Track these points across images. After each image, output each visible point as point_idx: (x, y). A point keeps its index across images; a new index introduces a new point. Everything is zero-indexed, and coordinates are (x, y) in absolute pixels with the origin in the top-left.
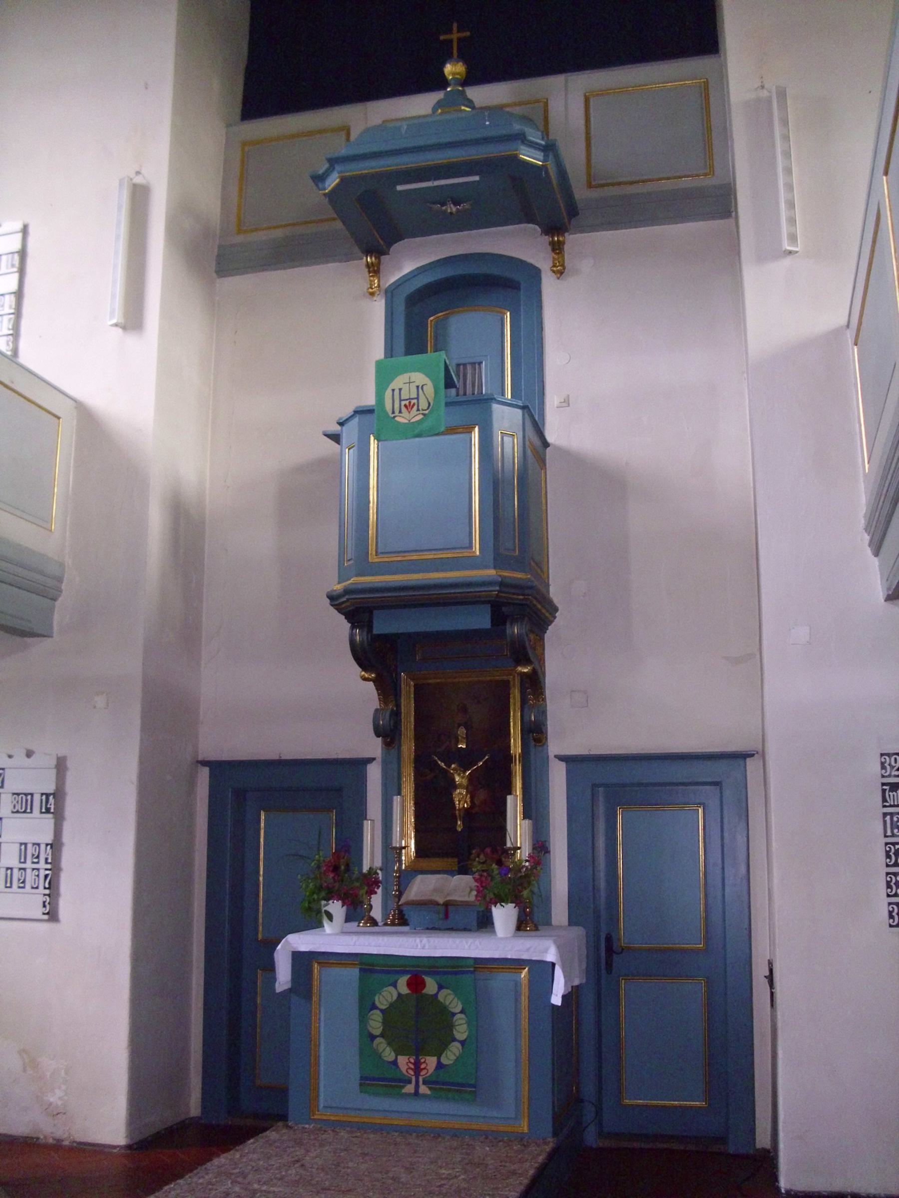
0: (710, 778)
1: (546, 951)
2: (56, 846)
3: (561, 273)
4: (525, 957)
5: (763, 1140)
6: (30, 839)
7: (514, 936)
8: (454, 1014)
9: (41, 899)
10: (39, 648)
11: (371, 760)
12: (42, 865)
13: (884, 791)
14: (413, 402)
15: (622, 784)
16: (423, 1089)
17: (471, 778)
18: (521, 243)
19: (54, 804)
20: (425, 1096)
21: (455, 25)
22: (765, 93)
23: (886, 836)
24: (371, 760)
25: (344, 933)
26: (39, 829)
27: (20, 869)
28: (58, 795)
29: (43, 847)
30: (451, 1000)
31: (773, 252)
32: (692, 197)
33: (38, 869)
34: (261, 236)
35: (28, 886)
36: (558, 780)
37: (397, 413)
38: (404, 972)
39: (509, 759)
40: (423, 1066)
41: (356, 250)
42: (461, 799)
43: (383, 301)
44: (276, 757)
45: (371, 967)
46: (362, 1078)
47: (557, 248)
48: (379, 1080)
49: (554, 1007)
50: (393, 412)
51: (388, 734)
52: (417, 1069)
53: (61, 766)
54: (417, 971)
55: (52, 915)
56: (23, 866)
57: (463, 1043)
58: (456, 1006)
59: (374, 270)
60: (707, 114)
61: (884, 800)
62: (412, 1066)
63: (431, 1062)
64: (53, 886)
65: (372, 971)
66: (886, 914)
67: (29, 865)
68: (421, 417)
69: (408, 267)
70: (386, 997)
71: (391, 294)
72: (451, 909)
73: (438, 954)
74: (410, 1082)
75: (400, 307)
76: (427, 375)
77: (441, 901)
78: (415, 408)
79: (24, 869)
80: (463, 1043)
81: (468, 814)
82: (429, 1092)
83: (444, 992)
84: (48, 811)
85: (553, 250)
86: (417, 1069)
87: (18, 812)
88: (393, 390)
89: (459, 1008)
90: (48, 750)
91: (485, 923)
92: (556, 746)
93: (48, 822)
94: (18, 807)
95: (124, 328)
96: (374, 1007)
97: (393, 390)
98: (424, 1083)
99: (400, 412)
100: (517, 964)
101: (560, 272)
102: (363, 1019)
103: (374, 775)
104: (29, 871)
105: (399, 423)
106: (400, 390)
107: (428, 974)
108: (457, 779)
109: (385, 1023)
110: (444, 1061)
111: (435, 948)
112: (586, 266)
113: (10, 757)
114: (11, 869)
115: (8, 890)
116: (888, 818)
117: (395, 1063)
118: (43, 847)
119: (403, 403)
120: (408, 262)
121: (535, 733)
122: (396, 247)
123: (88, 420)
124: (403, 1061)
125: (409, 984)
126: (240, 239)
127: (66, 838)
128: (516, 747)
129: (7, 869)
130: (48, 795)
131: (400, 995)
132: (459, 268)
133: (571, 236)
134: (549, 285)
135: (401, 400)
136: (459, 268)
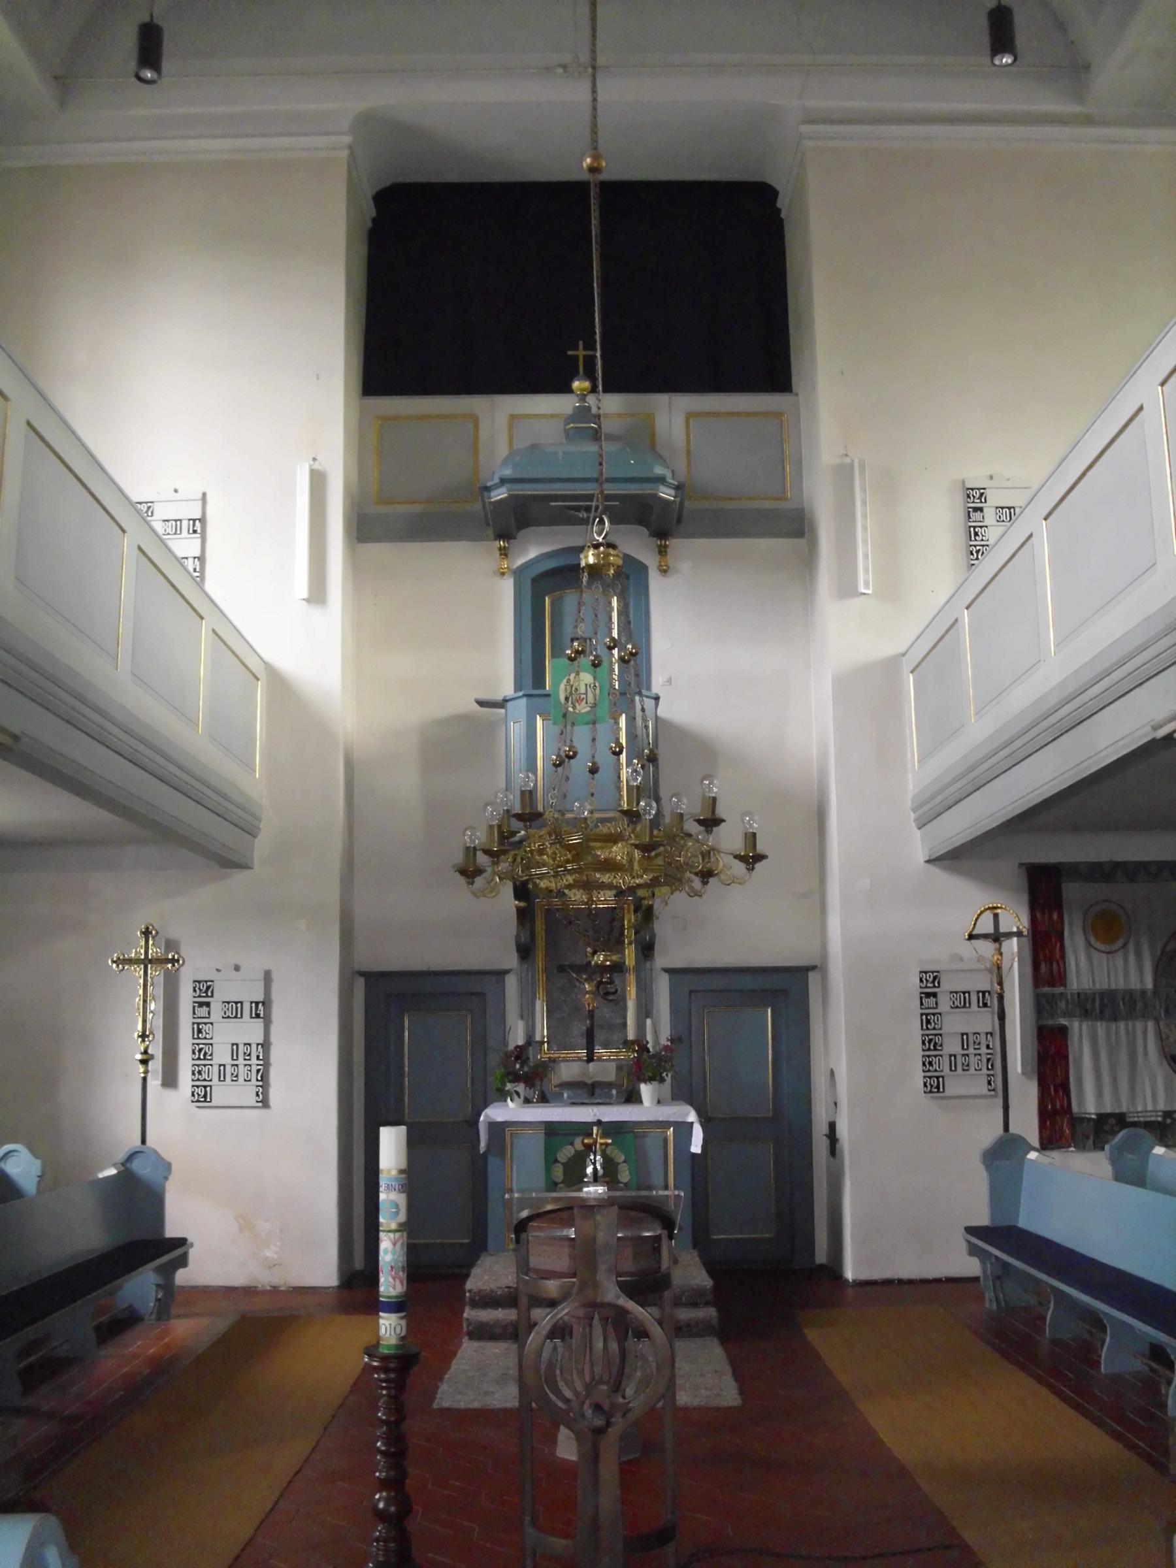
0: (784, 991)
1: (687, 1114)
2: (266, 1045)
3: (665, 571)
5: (821, 1257)
6: (241, 1040)
9: (255, 1089)
10: (239, 878)
11: (507, 972)
12: (254, 1061)
18: (636, 544)
19: (262, 1010)
21: (581, 343)
22: (847, 460)
24: (507, 972)
26: (250, 1031)
28: (266, 1003)
29: (254, 1047)
31: (847, 589)
32: (773, 523)
34: (401, 509)
35: (241, 1079)
36: (662, 988)
41: (490, 532)
43: (512, 580)
44: (423, 968)
45: (552, 1130)
47: (662, 551)
49: (694, 1155)
51: (525, 952)
53: (268, 977)
55: (265, 1103)
59: (504, 553)
60: (783, 451)
61: (922, 1004)
64: (264, 1078)
67: (241, 1061)
69: (533, 553)
71: (518, 573)
75: (528, 586)
77: (589, 1082)
84: (258, 1016)
85: (660, 552)
89: (623, 1158)
90: (254, 964)
91: (632, 1097)
92: (663, 959)
93: (259, 1024)
94: (957, 1003)
95: (308, 600)
96: (556, 1161)
100: (666, 1124)
101: (664, 571)
102: (548, 1171)
104: (972, 1057)
109: (565, 1173)
112: (684, 567)
113: (218, 970)
118: (254, 1047)
120: (533, 549)
121: (647, 950)
122: (521, 534)
123: (277, 681)
126: (382, 509)
127: (274, 1038)
130: (257, 1003)
132: (581, 564)
133: (1071, 885)
134: (656, 583)
136: (581, 564)
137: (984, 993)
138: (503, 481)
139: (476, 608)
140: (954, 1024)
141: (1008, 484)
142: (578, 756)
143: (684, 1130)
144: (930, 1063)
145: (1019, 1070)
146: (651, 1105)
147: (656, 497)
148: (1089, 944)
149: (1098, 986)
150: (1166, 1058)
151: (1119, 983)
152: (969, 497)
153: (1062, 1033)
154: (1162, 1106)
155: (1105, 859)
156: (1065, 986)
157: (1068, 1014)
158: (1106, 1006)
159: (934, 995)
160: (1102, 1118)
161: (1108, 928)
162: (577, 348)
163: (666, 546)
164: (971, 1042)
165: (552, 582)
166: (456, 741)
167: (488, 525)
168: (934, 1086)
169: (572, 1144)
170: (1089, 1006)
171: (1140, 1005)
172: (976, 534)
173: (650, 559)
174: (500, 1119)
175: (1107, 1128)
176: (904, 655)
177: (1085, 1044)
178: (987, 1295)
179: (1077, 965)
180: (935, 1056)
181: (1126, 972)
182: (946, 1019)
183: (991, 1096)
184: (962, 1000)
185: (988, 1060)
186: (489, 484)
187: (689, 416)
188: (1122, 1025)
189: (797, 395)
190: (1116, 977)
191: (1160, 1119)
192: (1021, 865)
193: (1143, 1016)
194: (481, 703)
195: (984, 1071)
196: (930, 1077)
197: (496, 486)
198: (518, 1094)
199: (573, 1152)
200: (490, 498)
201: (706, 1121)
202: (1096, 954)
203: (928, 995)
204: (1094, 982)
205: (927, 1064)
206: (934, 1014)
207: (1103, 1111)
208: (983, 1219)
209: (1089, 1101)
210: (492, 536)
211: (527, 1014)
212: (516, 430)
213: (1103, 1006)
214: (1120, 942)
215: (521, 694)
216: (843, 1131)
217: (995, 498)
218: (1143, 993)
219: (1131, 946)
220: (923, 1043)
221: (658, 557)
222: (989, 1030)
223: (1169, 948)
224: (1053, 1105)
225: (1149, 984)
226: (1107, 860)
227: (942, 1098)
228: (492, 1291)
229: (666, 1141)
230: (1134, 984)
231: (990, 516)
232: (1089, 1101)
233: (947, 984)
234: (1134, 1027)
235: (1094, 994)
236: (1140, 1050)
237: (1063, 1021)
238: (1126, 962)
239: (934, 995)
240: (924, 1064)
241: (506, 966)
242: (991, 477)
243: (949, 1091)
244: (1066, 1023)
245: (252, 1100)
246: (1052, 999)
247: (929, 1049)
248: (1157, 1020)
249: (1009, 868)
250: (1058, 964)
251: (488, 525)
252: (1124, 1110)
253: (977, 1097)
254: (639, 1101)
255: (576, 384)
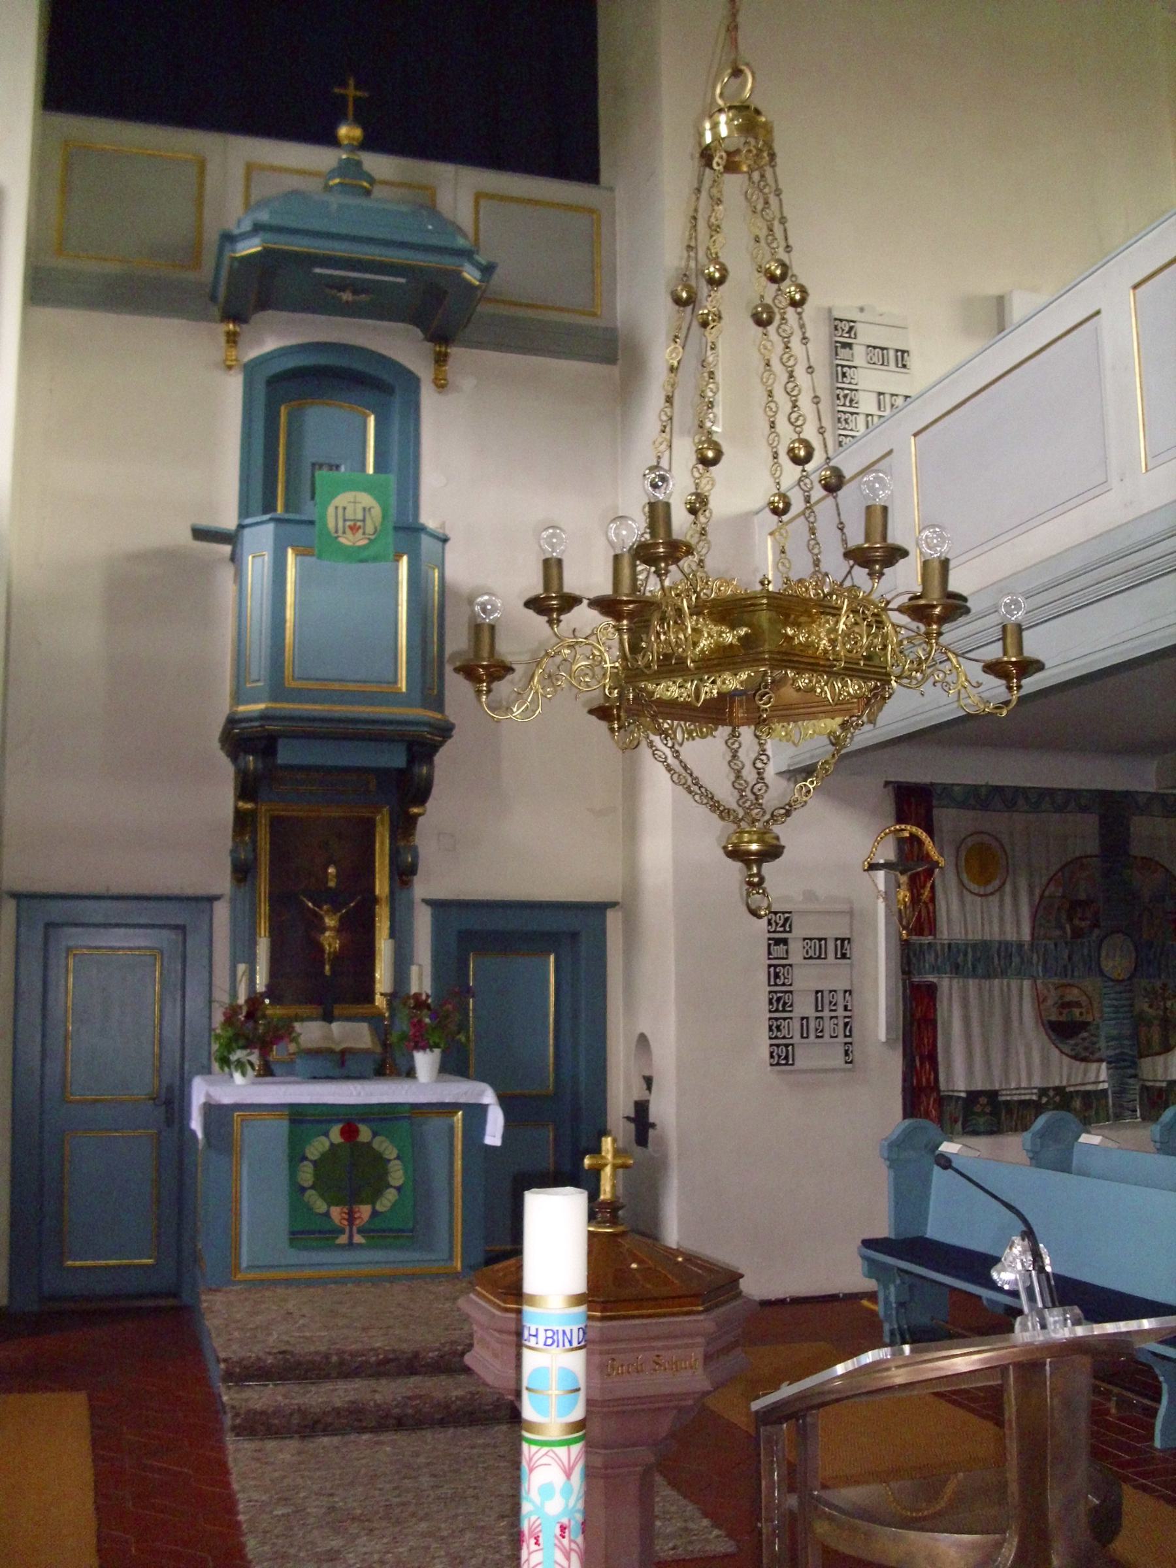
1: (481, 1094)
3: (442, 386)
4: (462, 1100)
6: (825, 986)
7: (438, 1081)
8: (389, 1161)
11: (217, 898)
13: (769, 945)
14: (359, 524)
15: (487, 933)
16: (358, 1239)
17: (342, 921)
20: (360, 1246)
23: (769, 985)
24: (217, 898)
25: (253, 1083)
27: (817, 1018)
30: (387, 1148)
33: (836, 1017)
35: (827, 1036)
37: (340, 533)
38: (339, 1121)
39: (375, 900)
40: (356, 1215)
41: (216, 311)
42: (330, 941)
46: (293, 1233)
47: (441, 359)
48: (308, 1232)
50: (336, 532)
51: (242, 872)
52: (351, 1219)
54: (350, 1119)
56: (819, 1014)
57: (399, 1189)
58: (390, 1152)
59: (232, 339)
61: (769, 953)
62: (346, 1216)
63: (365, 1211)
65: (301, 1122)
66: (767, 1055)
68: (366, 541)
69: (270, 345)
70: (317, 1147)
71: (250, 370)
72: (347, 1056)
73: (374, 1100)
74: (342, 1231)
76: (377, 499)
77: (338, 1048)
78: (361, 531)
79: (821, 1018)
80: (399, 1189)
81: (337, 958)
82: (363, 1241)
83: (378, 1139)
86: (351, 1219)
87: (811, 958)
88: (337, 508)
89: (394, 1155)
92: (423, 888)
94: (811, 953)
96: (304, 1158)
97: (337, 508)
98: (360, 1231)
99: (344, 532)
100: (449, 1109)
101: (441, 385)
103: (222, 913)
104: (827, 1021)
105: (341, 544)
106: (345, 509)
107: (363, 1121)
108: (327, 920)
109: (317, 1176)
110: (379, 1207)
111: (371, 1095)
112: (467, 383)
114: (807, 1018)
115: (820, 1040)
116: (772, 969)
117: (327, 1214)
119: (348, 523)
120: (272, 338)
121: (404, 873)
124: (337, 1213)
125: (343, 1133)
128: (382, 887)
129: (803, 1019)
131: (332, 1144)
135: (345, 520)
137: (843, 940)
138: (258, 228)
139: (189, 410)
140: (806, 979)
141: (878, 320)
142: (724, 460)
143: (476, 1114)
144: (778, 1028)
145: (882, 1036)
146: (426, 1081)
147: (457, 274)
148: (961, 882)
149: (970, 937)
150: (1043, 1025)
151: (993, 933)
152: (836, 328)
153: (930, 991)
154: (1037, 1082)
155: (981, 782)
156: (935, 935)
157: (935, 969)
158: (983, 960)
159: (785, 941)
160: (973, 1096)
161: (984, 864)
162: (344, 85)
163: (446, 355)
164: (826, 1002)
165: (285, 391)
166: (156, 586)
167: (213, 298)
168: (782, 1056)
169: (326, 1134)
170: (960, 960)
171: (1016, 960)
172: (844, 375)
173: (423, 370)
174: (226, 1100)
175: (978, 1109)
176: (757, 513)
177: (956, 1007)
178: (887, 1327)
179: (948, 911)
180: (785, 1019)
181: (1002, 920)
182: (796, 971)
183: (850, 1070)
184: (817, 948)
185: (846, 1024)
186: (236, 232)
187: (478, 197)
188: (996, 982)
189: (611, 189)
190: (991, 922)
191: (1034, 1098)
192: (887, 784)
193: (1019, 974)
194: (200, 534)
195: (841, 1039)
196: (778, 1046)
197: (244, 236)
198: (252, 1065)
199: (327, 1144)
200: (234, 251)
201: (505, 1101)
202: (969, 898)
203: (778, 942)
204: (966, 933)
205: (774, 1028)
206: (784, 966)
207: (973, 1088)
208: (883, 1229)
209: (958, 1076)
210: (218, 318)
211: (244, 952)
212: (253, 182)
213: (976, 960)
214: (996, 883)
215: (268, 517)
216: (663, 1110)
217: (866, 335)
218: (1020, 945)
219: (1008, 888)
220: (771, 1003)
221: (432, 366)
222: (848, 988)
223: (1047, 893)
224: (919, 1081)
225: (1026, 936)
226: (983, 783)
227: (791, 1072)
228: (259, 1359)
229: (452, 1128)
230: (1011, 936)
231: (859, 355)
232: (958, 1076)
233: (801, 929)
234: (1008, 985)
235: (967, 945)
236: (1015, 1016)
237: (931, 978)
238: (1001, 906)
239: (785, 941)
240: (771, 1029)
241: (215, 890)
242: (862, 310)
243: (799, 1064)
244: (935, 980)
245: (838, 1061)
246: (921, 951)
247: (777, 1010)
248: (1034, 979)
249: (873, 786)
250: (927, 907)
251: (213, 298)
252: (997, 1087)
253: (834, 1070)
254: (410, 1073)
255: (343, 131)
